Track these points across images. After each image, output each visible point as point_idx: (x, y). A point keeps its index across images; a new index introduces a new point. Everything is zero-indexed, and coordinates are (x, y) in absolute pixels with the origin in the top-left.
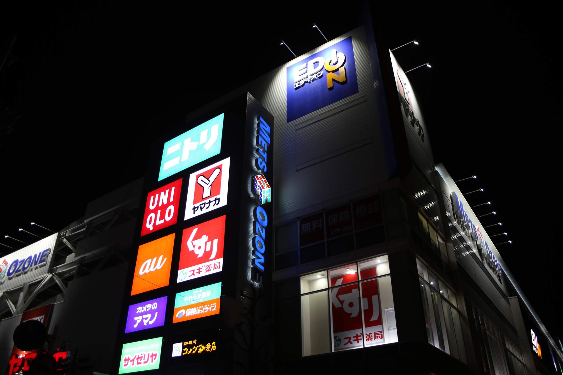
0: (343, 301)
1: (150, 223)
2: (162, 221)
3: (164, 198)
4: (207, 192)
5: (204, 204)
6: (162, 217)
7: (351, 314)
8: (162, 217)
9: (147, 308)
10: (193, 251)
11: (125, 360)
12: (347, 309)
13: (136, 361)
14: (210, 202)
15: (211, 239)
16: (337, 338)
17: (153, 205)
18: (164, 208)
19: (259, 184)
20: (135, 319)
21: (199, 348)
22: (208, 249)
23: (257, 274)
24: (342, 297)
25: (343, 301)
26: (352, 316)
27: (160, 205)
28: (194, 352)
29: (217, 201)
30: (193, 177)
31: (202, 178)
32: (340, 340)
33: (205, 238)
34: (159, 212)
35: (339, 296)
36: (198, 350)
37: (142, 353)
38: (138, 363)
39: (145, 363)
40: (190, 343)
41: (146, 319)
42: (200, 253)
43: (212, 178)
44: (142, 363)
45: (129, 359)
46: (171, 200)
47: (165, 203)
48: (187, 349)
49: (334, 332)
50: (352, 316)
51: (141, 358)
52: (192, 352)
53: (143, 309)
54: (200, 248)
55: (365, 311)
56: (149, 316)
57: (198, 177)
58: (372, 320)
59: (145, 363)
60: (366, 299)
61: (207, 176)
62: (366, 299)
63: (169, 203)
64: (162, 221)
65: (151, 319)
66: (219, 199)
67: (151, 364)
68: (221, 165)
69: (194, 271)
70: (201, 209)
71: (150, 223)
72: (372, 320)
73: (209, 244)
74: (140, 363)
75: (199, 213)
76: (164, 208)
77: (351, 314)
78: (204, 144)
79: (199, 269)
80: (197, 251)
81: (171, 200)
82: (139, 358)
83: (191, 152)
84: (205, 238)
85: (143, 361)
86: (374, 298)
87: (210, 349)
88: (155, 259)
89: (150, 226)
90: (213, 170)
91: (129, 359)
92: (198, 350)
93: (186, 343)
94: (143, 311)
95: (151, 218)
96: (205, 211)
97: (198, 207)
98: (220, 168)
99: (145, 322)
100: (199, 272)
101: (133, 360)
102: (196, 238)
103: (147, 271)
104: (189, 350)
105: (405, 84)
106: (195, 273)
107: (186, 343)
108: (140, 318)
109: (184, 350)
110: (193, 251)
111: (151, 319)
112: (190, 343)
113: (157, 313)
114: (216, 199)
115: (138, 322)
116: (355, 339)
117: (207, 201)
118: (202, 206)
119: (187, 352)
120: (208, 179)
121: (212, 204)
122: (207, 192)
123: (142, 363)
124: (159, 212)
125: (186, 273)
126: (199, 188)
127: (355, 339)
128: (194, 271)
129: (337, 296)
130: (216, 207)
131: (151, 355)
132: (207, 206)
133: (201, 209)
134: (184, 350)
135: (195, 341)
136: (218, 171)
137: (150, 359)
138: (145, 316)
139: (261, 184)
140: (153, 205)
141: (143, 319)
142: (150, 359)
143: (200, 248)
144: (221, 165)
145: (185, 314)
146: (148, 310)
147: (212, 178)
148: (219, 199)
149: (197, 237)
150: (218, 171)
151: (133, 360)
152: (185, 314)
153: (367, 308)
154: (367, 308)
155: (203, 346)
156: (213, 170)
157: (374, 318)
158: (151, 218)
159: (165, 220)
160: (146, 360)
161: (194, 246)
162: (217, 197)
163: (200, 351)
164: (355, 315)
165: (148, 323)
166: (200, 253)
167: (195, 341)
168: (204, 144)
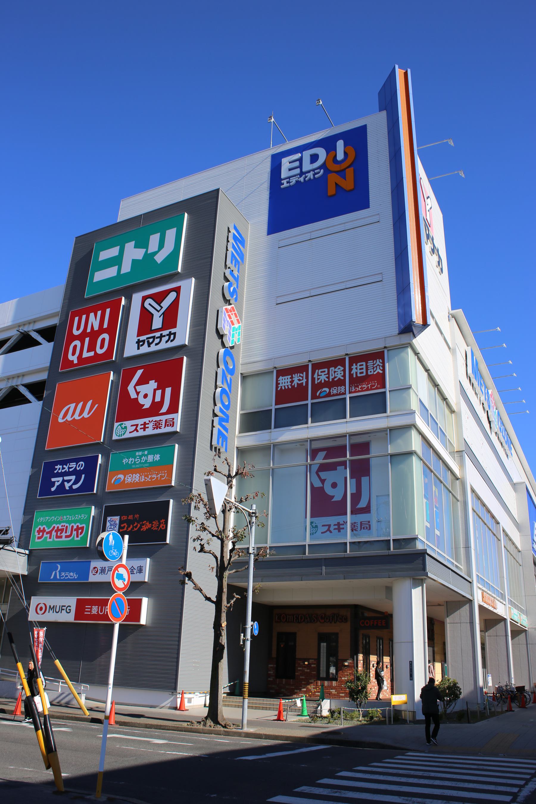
0: (325, 480)
1: (73, 354)
2: (92, 354)
3: (94, 321)
4: (157, 323)
5: (154, 337)
6: (92, 347)
7: (333, 497)
8: (92, 347)
9: (69, 468)
10: (136, 399)
11: (39, 531)
12: (329, 490)
13: (54, 533)
14: (161, 336)
15: (161, 387)
16: (314, 525)
17: (78, 329)
18: (94, 335)
19: (228, 319)
20: (53, 480)
21: (143, 525)
22: (158, 399)
23: (221, 440)
24: (323, 475)
25: (325, 480)
26: (334, 500)
27: (89, 330)
28: (135, 529)
29: (172, 336)
30: (137, 298)
31: (149, 301)
32: (316, 527)
33: (153, 384)
34: (87, 340)
35: (320, 473)
36: (141, 528)
37: (63, 524)
38: (57, 537)
39: (67, 537)
40: (131, 517)
41: (69, 481)
42: (147, 403)
43: (167, 303)
44: (64, 537)
45: (44, 530)
46: (105, 326)
47: (96, 328)
48: (125, 524)
49: (312, 516)
50: (334, 500)
51: (62, 530)
52: (133, 529)
53: (63, 468)
54: (146, 396)
55: (352, 495)
56: (73, 478)
57: (144, 299)
58: (359, 506)
59: (67, 537)
60: (354, 480)
61: (159, 298)
62: (354, 480)
63: (101, 330)
64: (92, 354)
65: (76, 483)
66: (175, 334)
67: (76, 539)
68: (179, 287)
69: (137, 425)
70: (149, 345)
71: (73, 354)
72: (359, 506)
73: (159, 393)
74: (61, 537)
75: (145, 349)
76: (94, 335)
77: (333, 497)
78: (155, 253)
79: (145, 424)
80: (141, 400)
81: (105, 326)
82: (58, 530)
83: (135, 262)
84: (153, 384)
85: (64, 534)
86: (365, 480)
87: (158, 527)
88: (81, 404)
89: (74, 359)
90: (166, 293)
91: (44, 530)
92: (141, 528)
93: (125, 518)
94: (63, 471)
95: (75, 347)
96: (153, 348)
97: (144, 341)
98: (177, 290)
99: (67, 486)
100: (144, 429)
101: (50, 533)
102: (139, 383)
103: (69, 418)
104: (129, 526)
105: (428, 197)
106: (138, 428)
107: (125, 518)
108: (61, 479)
109: (122, 525)
110: (136, 399)
111: (76, 483)
112: (131, 517)
113: (83, 476)
114: (170, 334)
115: (57, 484)
116: (336, 527)
117: (158, 334)
118: (151, 340)
119: (125, 529)
120: (159, 304)
121: (165, 339)
122: (157, 323)
123: (64, 537)
124: (87, 340)
125: (126, 427)
126: (146, 317)
127: (336, 527)
128: (137, 425)
129: (317, 473)
130: (170, 345)
131: (75, 527)
132: (157, 341)
133: (149, 345)
134: (122, 525)
135: (137, 516)
136: (172, 296)
137: (75, 533)
138: (66, 478)
139: (230, 318)
140: (78, 329)
141: (64, 481)
142: (75, 533)
143: (146, 396)
144: (179, 287)
145: (124, 480)
146: (71, 470)
147: (167, 303)
148: (175, 334)
149: (142, 381)
150: (172, 296)
151: (50, 533)
152: (124, 480)
153: (355, 492)
154: (355, 492)
155: (148, 524)
156: (166, 293)
157: (362, 504)
158: (75, 347)
159: (96, 353)
160: (68, 534)
161: (138, 393)
162: (173, 330)
163: (144, 528)
164: (338, 498)
165: (71, 487)
166: (147, 403)
167: (137, 516)
168: (155, 253)
